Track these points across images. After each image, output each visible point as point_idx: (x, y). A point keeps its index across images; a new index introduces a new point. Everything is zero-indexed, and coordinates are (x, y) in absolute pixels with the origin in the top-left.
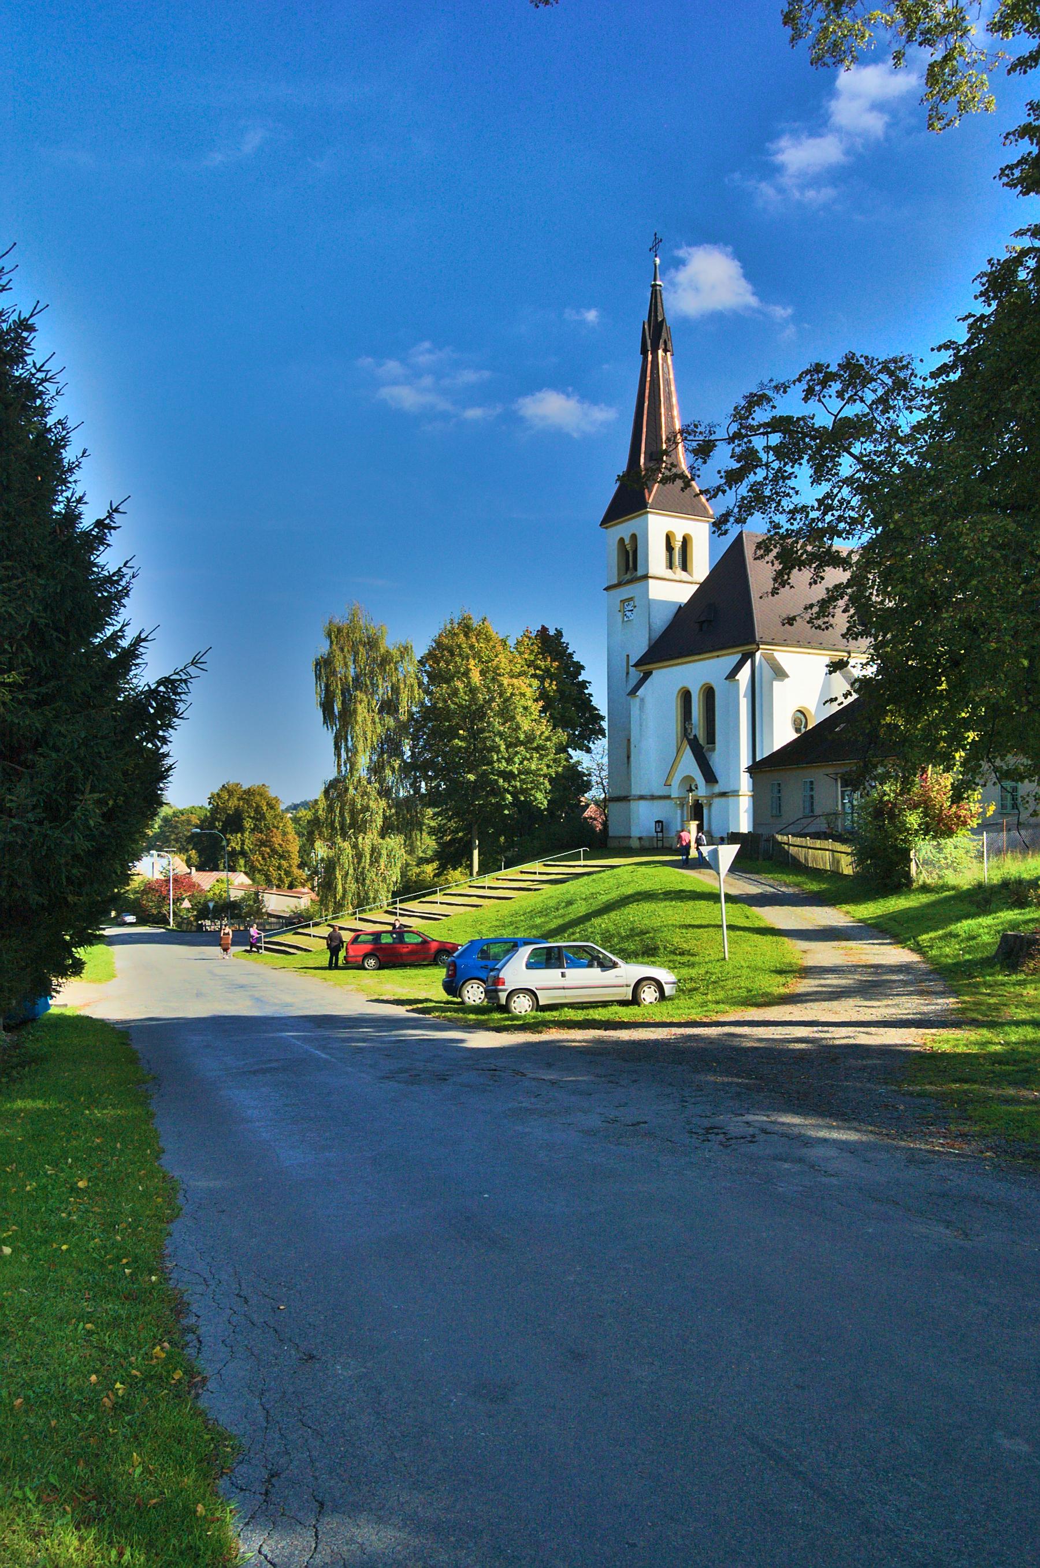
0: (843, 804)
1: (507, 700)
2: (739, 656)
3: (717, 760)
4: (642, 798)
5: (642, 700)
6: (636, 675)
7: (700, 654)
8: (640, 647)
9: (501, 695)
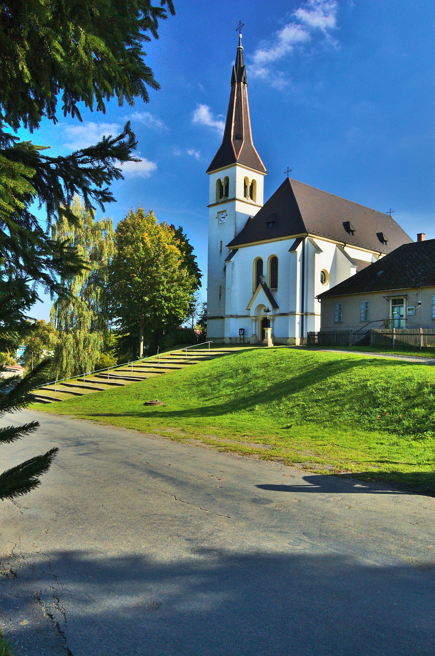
0: (393, 314)
1: (168, 256)
2: (294, 240)
3: (279, 296)
4: (232, 316)
5: (233, 264)
6: (226, 251)
7: (270, 239)
8: (230, 237)
9: (164, 252)
